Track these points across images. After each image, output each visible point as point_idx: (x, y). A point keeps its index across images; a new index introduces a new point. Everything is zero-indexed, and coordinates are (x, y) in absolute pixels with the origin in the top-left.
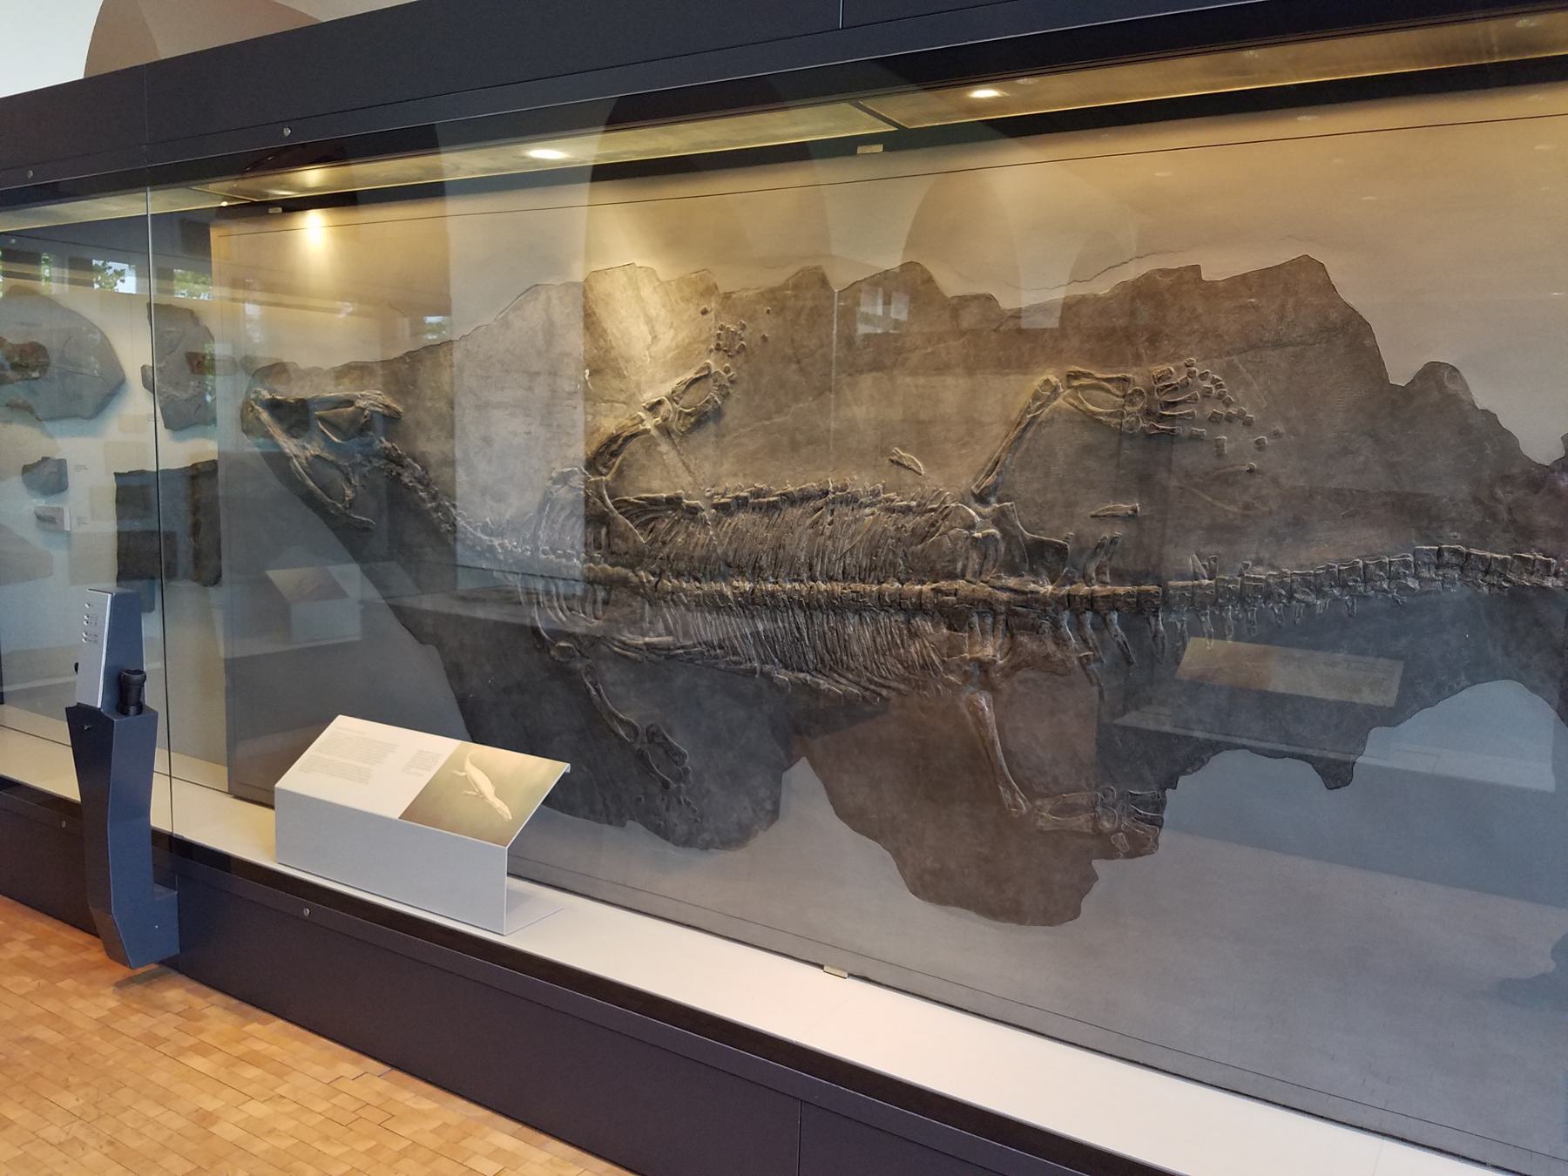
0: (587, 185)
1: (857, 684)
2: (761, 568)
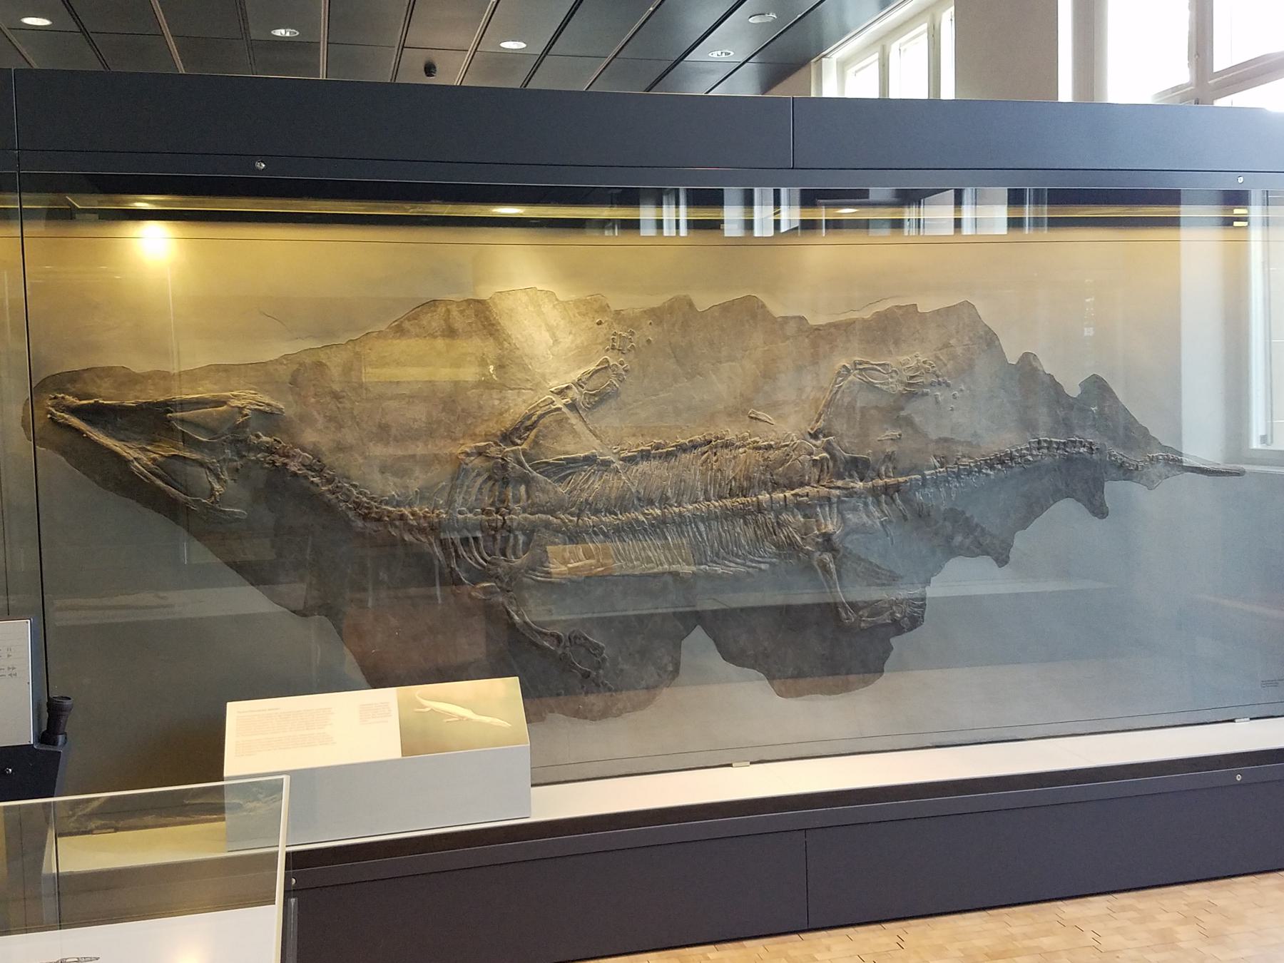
0: (43, 222)
1: (743, 565)
2: (668, 498)
